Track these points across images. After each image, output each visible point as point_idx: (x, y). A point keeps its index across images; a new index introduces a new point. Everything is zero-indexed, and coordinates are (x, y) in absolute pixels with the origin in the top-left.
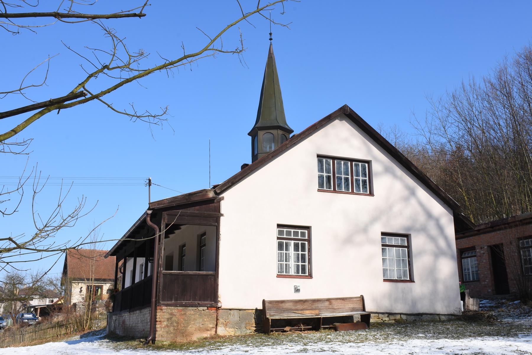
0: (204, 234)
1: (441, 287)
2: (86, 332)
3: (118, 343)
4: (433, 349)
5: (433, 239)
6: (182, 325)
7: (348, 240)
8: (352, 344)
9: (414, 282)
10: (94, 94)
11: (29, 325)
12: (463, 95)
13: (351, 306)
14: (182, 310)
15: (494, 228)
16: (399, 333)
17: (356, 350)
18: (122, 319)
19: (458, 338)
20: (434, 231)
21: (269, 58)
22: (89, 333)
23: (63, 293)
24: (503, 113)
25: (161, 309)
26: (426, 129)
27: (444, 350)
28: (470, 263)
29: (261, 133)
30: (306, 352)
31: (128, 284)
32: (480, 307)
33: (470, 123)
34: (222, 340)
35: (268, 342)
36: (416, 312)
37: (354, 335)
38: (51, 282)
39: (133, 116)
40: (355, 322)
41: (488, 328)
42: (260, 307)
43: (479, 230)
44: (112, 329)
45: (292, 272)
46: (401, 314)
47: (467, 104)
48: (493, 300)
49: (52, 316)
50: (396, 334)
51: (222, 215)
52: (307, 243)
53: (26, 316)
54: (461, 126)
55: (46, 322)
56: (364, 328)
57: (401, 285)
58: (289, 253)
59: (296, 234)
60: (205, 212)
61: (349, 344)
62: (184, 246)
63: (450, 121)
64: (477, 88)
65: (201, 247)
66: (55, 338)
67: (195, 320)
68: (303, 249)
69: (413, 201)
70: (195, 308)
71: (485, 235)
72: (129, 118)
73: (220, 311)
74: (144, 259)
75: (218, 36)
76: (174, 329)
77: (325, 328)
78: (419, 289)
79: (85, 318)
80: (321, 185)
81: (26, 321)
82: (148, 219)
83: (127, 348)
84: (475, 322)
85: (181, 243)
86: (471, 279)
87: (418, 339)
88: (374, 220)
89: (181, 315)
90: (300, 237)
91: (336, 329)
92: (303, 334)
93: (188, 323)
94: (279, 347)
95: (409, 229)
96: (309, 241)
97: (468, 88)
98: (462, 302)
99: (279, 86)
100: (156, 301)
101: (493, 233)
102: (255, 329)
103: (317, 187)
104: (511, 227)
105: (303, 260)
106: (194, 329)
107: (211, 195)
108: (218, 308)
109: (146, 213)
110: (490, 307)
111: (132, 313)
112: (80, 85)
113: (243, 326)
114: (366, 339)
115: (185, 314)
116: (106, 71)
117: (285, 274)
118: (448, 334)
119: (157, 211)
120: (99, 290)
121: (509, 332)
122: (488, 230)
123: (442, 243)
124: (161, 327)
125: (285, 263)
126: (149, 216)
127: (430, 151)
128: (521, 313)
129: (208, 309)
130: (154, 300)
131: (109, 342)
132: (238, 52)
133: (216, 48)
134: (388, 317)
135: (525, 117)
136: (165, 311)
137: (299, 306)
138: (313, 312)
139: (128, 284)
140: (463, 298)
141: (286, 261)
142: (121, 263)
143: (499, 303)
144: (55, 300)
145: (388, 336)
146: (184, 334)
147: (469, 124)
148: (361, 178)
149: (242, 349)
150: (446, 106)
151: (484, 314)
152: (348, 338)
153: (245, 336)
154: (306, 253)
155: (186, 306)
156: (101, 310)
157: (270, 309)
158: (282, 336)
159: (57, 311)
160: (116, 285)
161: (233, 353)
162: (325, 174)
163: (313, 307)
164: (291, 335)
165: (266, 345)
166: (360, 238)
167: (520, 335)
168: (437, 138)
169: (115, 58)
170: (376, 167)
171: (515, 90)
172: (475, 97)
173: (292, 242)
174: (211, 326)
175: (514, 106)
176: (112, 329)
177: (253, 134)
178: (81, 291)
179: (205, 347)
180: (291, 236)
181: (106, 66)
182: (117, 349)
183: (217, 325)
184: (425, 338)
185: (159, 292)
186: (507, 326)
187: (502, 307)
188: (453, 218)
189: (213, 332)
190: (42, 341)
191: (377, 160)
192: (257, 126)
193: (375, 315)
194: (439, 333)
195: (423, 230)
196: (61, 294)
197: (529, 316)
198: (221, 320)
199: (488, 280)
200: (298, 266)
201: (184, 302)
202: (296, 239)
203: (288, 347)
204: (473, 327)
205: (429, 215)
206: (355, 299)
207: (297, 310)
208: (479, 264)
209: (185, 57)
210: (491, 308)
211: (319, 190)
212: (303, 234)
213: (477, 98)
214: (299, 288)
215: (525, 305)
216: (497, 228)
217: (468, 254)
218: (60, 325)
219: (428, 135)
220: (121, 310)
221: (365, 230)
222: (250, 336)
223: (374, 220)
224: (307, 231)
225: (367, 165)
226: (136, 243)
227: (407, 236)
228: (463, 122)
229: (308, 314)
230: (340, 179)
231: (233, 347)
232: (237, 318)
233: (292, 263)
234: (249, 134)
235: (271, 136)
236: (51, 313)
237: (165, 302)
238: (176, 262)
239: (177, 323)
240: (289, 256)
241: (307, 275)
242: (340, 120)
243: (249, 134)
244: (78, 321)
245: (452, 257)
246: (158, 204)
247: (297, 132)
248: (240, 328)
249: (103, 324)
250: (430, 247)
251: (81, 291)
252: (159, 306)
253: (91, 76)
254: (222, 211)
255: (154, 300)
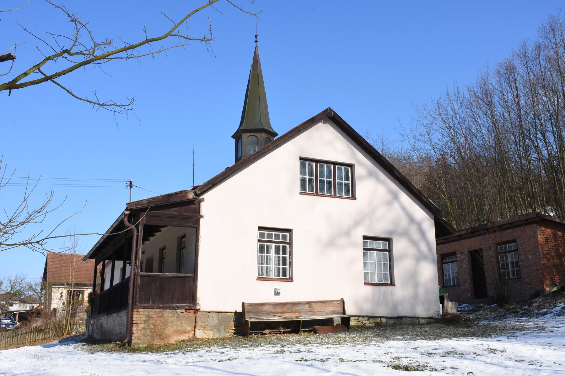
0: (184, 236)
1: (421, 291)
2: (65, 337)
3: (94, 346)
4: (408, 349)
5: (414, 243)
6: (160, 328)
7: (331, 243)
8: (330, 346)
9: (394, 285)
10: (48, 74)
11: (7, 331)
12: (447, 103)
13: (331, 309)
14: (159, 313)
15: (475, 234)
16: (378, 335)
17: (333, 350)
18: (99, 323)
19: (435, 339)
20: (416, 235)
21: (254, 60)
22: (68, 338)
23: (43, 298)
24: (485, 123)
25: (138, 312)
26: (411, 136)
27: (419, 350)
28: (451, 268)
29: (245, 136)
30: (283, 353)
31: (107, 286)
32: (458, 311)
33: (454, 130)
34: (199, 342)
35: (246, 344)
36: (396, 315)
37: (333, 337)
38: (31, 287)
39: (95, 104)
40: (335, 325)
41: (465, 330)
42: (240, 310)
43: (460, 236)
44: (90, 333)
45: (273, 275)
46: (381, 317)
47: (451, 112)
48: (471, 304)
49: (30, 322)
50: (374, 337)
51: (202, 217)
52: (288, 246)
53: (4, 321)
54: (445, 134)
55: (24, 327)
56: (344, 331)
57: (383, 288)
58: (270, 256)
59: (277, 236)
60: (185, 214)
61: (327, 346)
62: (164, 248)
63: (435, 128)
64: (461, 95)
65: (181, 249)
66: (33, 343)
67: (172, 322)
68: (284, 252)
69: (396, 206)
70: (173, 311)
71: (465, 240)
72: (91, 105)
73: (199, 314)
74: (122, 262)
75: (182, 21)
76: (151, 332)
77: (304, 331)
78: (400, 292)
79: (64, 323)
80: (303, 186)
81: (4, 326)
82: (126, 219)
83: (102, 351)
84: (452, 324)
85: (161, 246)
86: (452, 284)
87: (396, 340)
88: (357, 223)
89: (159, 317)
90: (281, 240)
91: (315, 332)
92: (282, 337)
93: (165, 326)
94: (256, 349)
95: (392, 233)
96: (291, 244)
97: (452, 95)
98: (441, 305)
99: (263, 88)
100: (132, 303)
101: (473, 239)
102: (234, 331)
103: (299, 189)
104: (490, 233)
105: (284, 263)
106: (171, 331)
107: (191, 196)
108: (196, 311)
109: (123, 214)
110: (468, 311)
111: (109, 316)
112: (35, 66)
113: (222, 328)
114: (345, 341)
115: (162, 316)
116: (66, 55)
117: (265, 276)
118: (425, 336)
119: (134, 212)
120: (81, 295)
121: (484, 333)
122: (469, 235)
123: (423, 247)
124: (138, 330)
125: (265, 266)
126: (127, 216)
127: (415, 157)
128: (497, 316)
129: (186, 311)
130: (130, 302)
131: (85, 345)
132: (204, 40)
133: (181, 35)
134: (368, 320)
135: (505, 126)
136: (142, 313)
137: (279, 309)
138: (293, 315)
139: (107, 286)
140: (442, 302)
141: (267, 264)
142: (100, 266)
143: (477, 307)
144: (36, 306)
145: (366, 338)
146: (161, 336)
147: (453, 131)
148: (344, 182)
149: (218, 350)
150: (431, 113)
151: (462, 317)
152: (326, 340)
153: (223, 339)
154: (288, 256)
155: (163, 308)
156: (82, 315)
157: (249, 312)
158: (261, 338)
159: (35, 315)
160: (94, 289)
161: (209, 354)
162: (307, 177)
163: (293, 310)
164: (270, 338)
165: (243, 347)
166: (341, 241)
167: (493, 336)
168: (421, 144)
169: (76, 44)
170: (359, 171)
171: (496, 99)
172: (460, 105)
173: (273, 245)
174: (189, 328)
175: (496, 114)
176: (90, 333)
177: (237, 136)
178: (61, 296)
179: (181, 349)
180: (272, 238)
181: (66, 50)
182: (91, 352)
183: (195, 328)
184: (403, 340)
185: (136, 294)
186: (483, 328)
187: (480, 311)
188: (434, 222)
189: (191, 335)
190: (18, 345)
191: (360, 163)
192: (241, 128)
193: (355, 318)
194: (417, 335)
195: (405, 234)
196: (40, 299)
197: (504, 318)
198: (199, 323)
199: (467, 285)
200: (279, 269)
201: (161, 305)
202: (277, 243)
203: (265, 348)
204: (452, 329)
205: (412, 219)
206: (335, 302)
207: (277, 313)
208: (459, 269)
209: (148, 41)
210: (470, 312)
211: (301, 193)
212: (284, 237)
213: (461, 106)
214: (279, 291)
215: (501, 308)
216: (478, 233)
217: (450, 258)
218: (38, 330)
219: (412, 141)
220: (99, 313)
221: (348, 233)
222: (229, 339)
223: (357, 223)
224: (288, 234)
225: (350, 169)
226: (114, 246)
227: (389, 240)
228: (447, 130)
229: (288, 317)
230: (322, 182)
231: (210, 349)
232: (215, 321)
233: (273, 266)
234: (233, 137)
235: (255, 138)
236: (30, 318)
237: (142, 305)
238: (156, 265)
239: (155, 325)
240: (270, 259)
241: (288, 277)
242: (324, 123)
243: (233, 137)
244: (57, 326)
245: (433, 261)
246: (136, 205)
247: (280, 134)
248: (219, 331)
249: (83, 329)
250: (412, 250)
251: (61, 296)
252: (135, 308)
253: (48, 59)
254: (202, 213)
255: (130, 302)
